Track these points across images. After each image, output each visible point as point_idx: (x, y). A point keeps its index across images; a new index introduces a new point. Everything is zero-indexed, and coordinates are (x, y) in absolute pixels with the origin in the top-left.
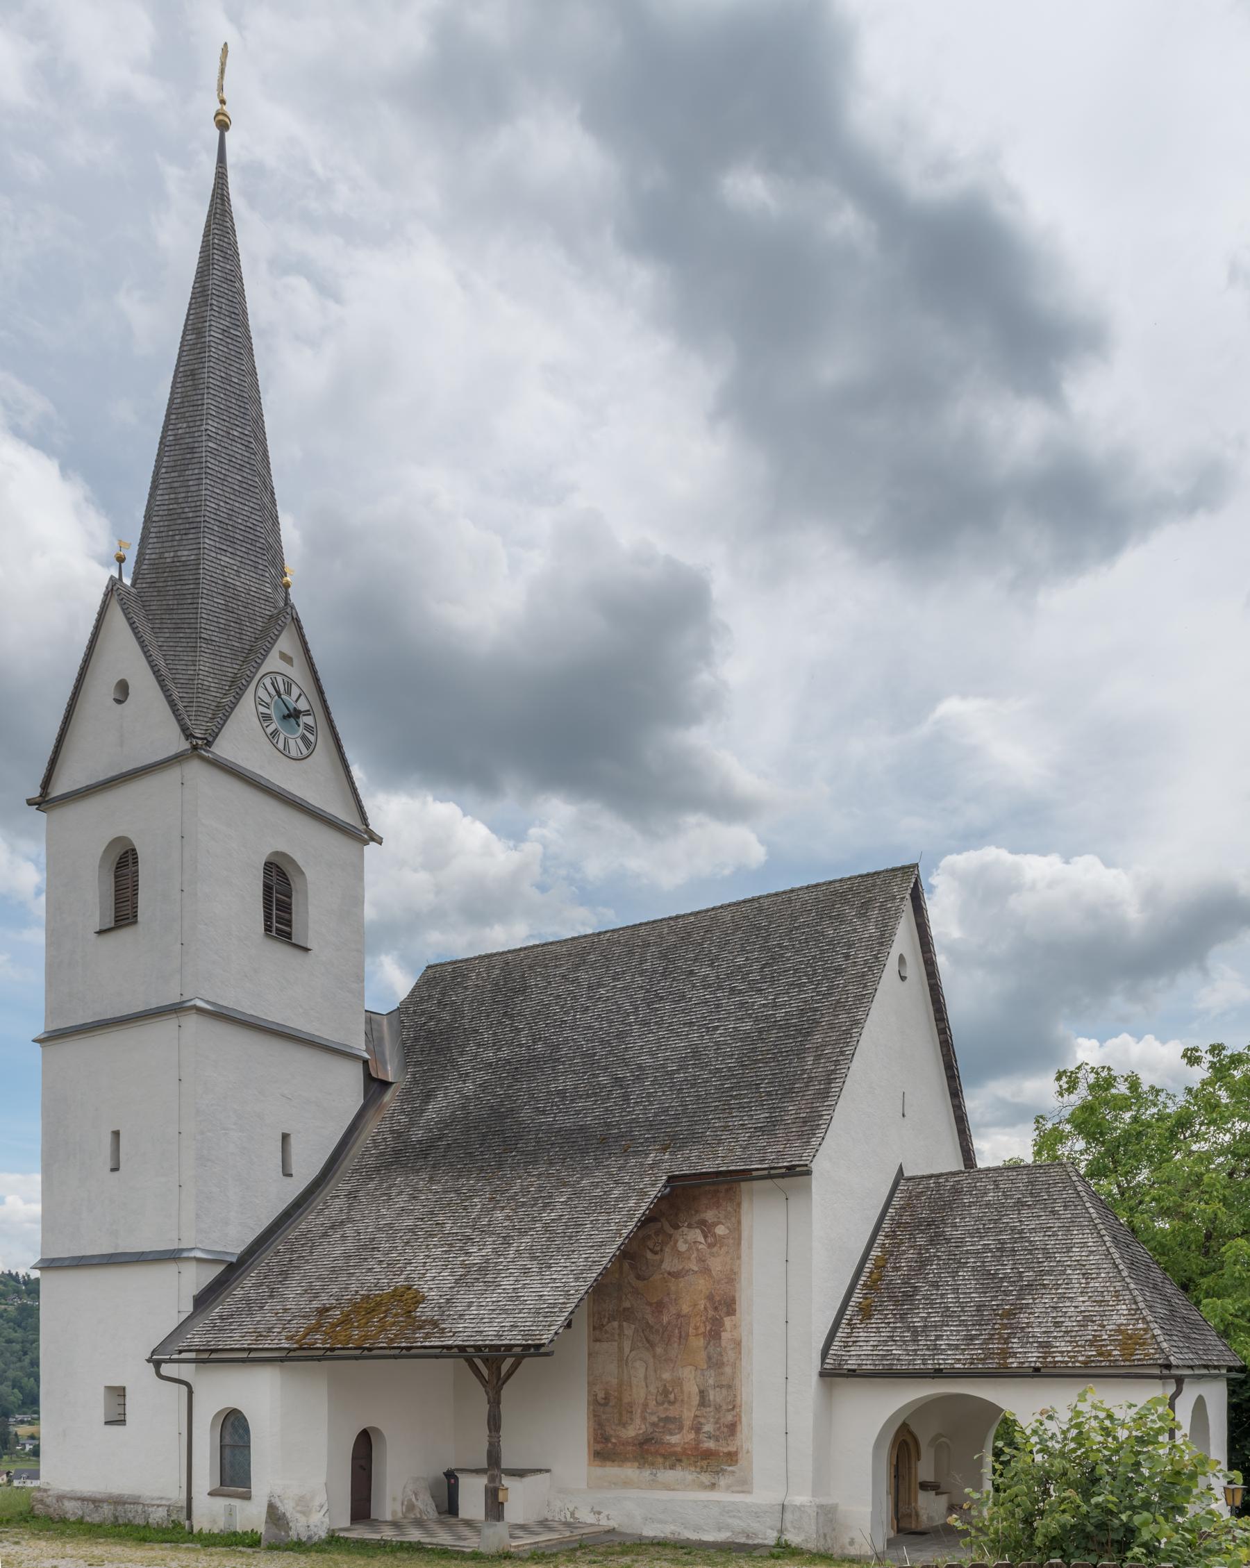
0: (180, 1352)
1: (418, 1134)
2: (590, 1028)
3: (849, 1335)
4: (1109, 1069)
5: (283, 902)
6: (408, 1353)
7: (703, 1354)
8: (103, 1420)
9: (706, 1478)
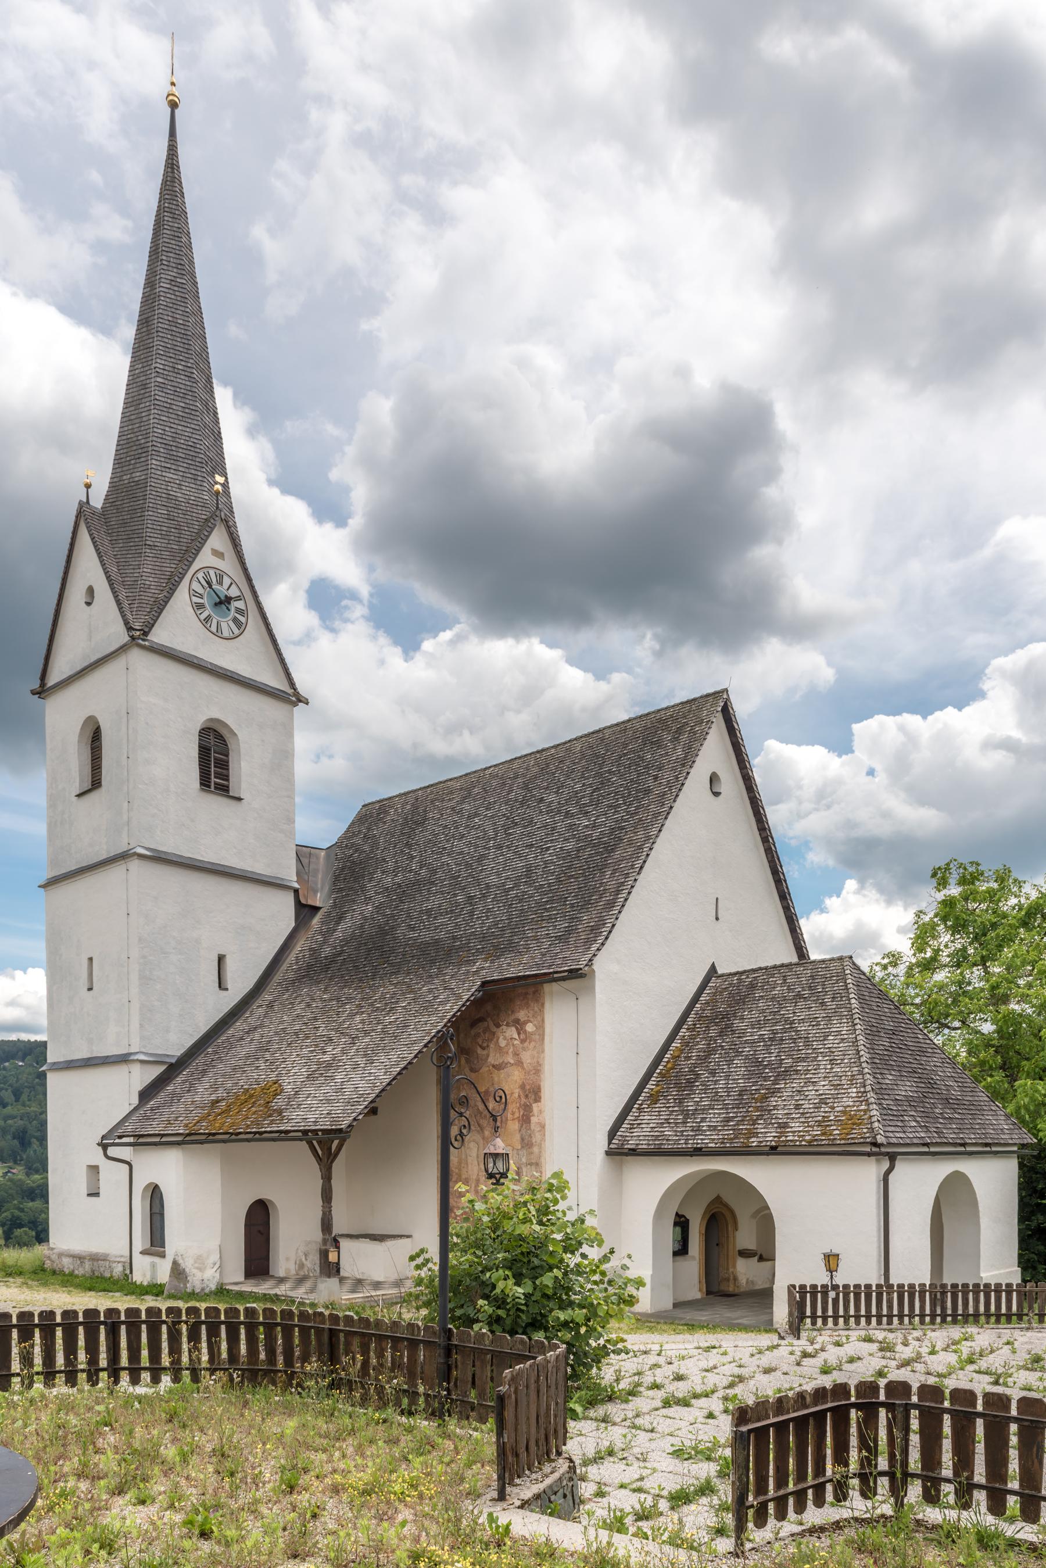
0: (120, 1137)
1: (327, 951)
2: (461, 853)
3: (637, 1118)
4: (978, 864)
5: (221, 760)
6: (259, 1137)
7: (518, 1137)
8: (86, 1193)
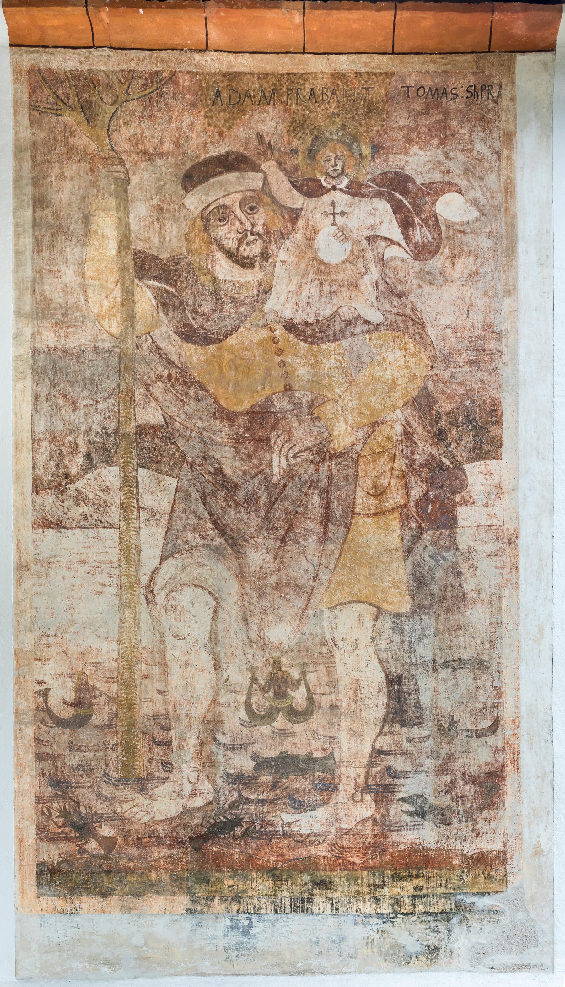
7: (400, 571)
9: (408, 934)
